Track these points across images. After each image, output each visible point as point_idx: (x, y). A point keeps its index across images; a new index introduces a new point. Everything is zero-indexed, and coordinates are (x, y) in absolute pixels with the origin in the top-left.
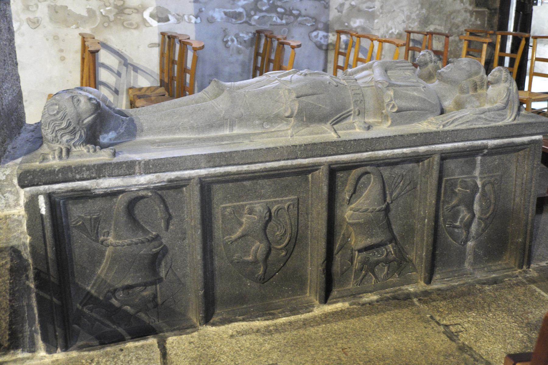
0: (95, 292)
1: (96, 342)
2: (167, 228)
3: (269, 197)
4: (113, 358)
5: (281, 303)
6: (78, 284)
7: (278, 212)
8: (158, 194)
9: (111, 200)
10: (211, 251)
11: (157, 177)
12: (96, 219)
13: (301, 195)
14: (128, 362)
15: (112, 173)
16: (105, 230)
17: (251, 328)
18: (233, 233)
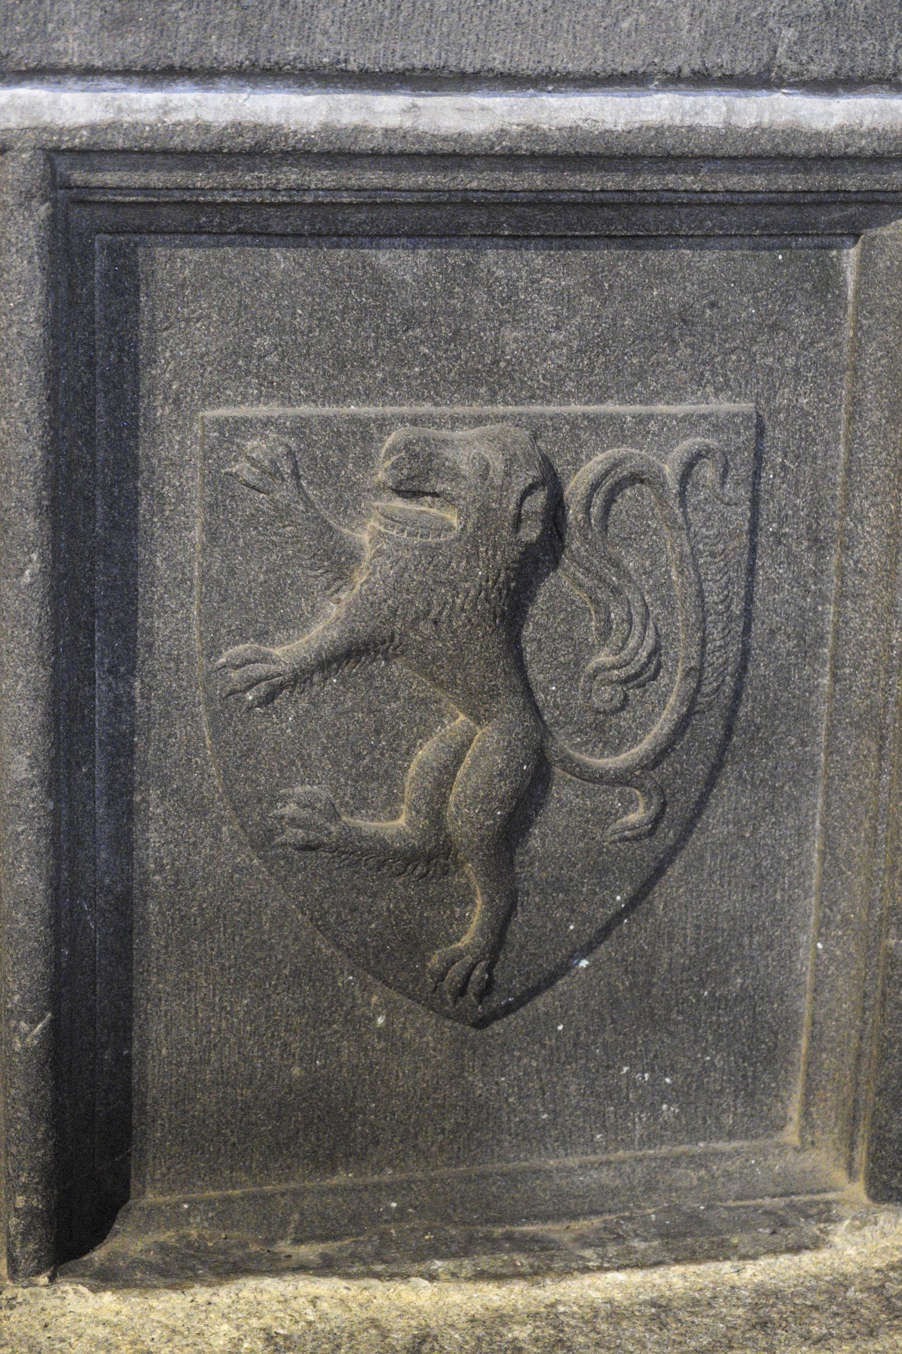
3: (553, 389)
5: (605, 1177)
7: (610, 501)
10: (123, 748)
13: (782, 399)
17: (374, 1323)
18: (284, 623)
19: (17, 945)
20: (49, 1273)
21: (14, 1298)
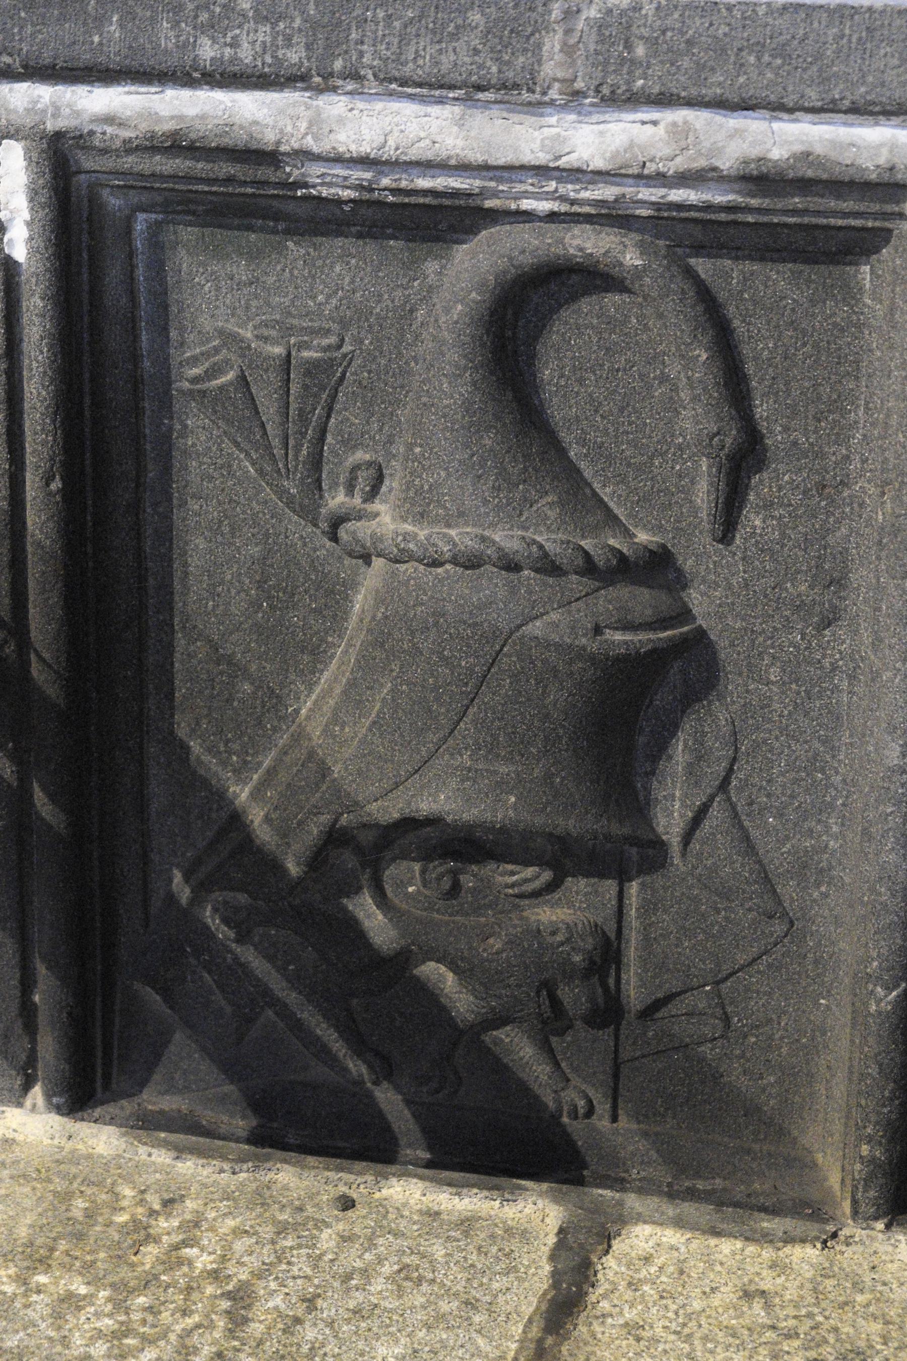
0: (267, 819)
1: (242, 1124)
2: (728, 521)
4: (282, 1229)
6: (186, 749)
8: (690, 273)
9: (412, 265)
11: (679, 132)
12: (312, 369)
14: (348, 1277)
15: (399, 60)
16: (361, 456)
19: (879, 916)
20: (886, 1220)
21: (851, 1237)
